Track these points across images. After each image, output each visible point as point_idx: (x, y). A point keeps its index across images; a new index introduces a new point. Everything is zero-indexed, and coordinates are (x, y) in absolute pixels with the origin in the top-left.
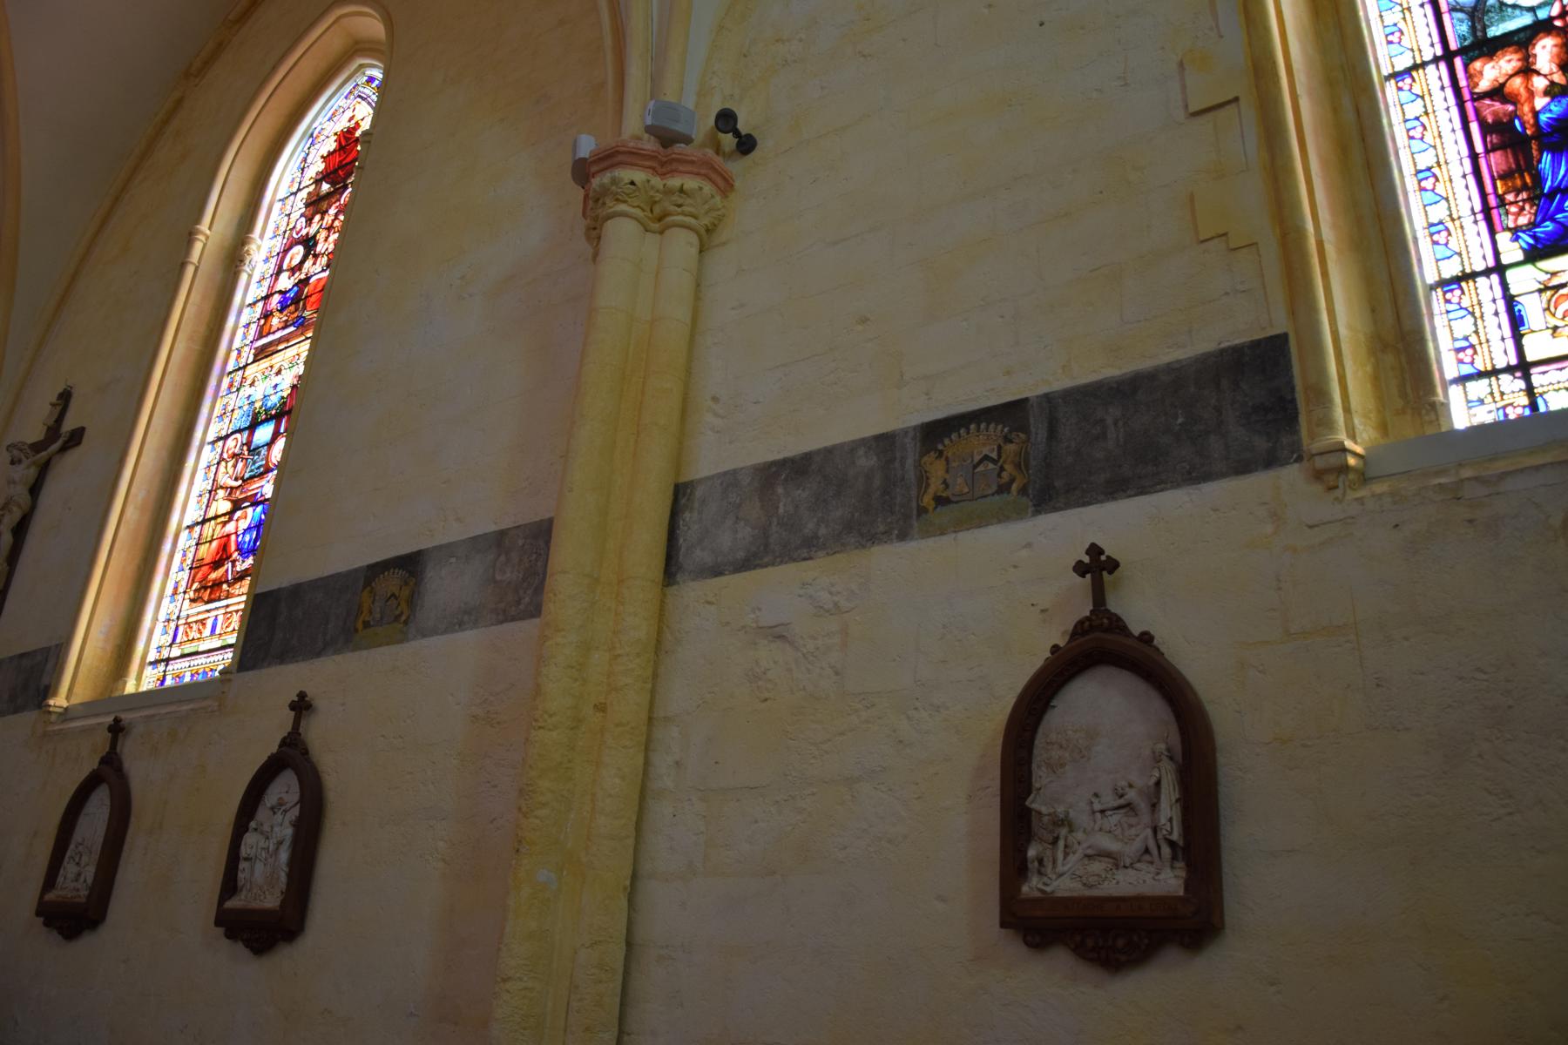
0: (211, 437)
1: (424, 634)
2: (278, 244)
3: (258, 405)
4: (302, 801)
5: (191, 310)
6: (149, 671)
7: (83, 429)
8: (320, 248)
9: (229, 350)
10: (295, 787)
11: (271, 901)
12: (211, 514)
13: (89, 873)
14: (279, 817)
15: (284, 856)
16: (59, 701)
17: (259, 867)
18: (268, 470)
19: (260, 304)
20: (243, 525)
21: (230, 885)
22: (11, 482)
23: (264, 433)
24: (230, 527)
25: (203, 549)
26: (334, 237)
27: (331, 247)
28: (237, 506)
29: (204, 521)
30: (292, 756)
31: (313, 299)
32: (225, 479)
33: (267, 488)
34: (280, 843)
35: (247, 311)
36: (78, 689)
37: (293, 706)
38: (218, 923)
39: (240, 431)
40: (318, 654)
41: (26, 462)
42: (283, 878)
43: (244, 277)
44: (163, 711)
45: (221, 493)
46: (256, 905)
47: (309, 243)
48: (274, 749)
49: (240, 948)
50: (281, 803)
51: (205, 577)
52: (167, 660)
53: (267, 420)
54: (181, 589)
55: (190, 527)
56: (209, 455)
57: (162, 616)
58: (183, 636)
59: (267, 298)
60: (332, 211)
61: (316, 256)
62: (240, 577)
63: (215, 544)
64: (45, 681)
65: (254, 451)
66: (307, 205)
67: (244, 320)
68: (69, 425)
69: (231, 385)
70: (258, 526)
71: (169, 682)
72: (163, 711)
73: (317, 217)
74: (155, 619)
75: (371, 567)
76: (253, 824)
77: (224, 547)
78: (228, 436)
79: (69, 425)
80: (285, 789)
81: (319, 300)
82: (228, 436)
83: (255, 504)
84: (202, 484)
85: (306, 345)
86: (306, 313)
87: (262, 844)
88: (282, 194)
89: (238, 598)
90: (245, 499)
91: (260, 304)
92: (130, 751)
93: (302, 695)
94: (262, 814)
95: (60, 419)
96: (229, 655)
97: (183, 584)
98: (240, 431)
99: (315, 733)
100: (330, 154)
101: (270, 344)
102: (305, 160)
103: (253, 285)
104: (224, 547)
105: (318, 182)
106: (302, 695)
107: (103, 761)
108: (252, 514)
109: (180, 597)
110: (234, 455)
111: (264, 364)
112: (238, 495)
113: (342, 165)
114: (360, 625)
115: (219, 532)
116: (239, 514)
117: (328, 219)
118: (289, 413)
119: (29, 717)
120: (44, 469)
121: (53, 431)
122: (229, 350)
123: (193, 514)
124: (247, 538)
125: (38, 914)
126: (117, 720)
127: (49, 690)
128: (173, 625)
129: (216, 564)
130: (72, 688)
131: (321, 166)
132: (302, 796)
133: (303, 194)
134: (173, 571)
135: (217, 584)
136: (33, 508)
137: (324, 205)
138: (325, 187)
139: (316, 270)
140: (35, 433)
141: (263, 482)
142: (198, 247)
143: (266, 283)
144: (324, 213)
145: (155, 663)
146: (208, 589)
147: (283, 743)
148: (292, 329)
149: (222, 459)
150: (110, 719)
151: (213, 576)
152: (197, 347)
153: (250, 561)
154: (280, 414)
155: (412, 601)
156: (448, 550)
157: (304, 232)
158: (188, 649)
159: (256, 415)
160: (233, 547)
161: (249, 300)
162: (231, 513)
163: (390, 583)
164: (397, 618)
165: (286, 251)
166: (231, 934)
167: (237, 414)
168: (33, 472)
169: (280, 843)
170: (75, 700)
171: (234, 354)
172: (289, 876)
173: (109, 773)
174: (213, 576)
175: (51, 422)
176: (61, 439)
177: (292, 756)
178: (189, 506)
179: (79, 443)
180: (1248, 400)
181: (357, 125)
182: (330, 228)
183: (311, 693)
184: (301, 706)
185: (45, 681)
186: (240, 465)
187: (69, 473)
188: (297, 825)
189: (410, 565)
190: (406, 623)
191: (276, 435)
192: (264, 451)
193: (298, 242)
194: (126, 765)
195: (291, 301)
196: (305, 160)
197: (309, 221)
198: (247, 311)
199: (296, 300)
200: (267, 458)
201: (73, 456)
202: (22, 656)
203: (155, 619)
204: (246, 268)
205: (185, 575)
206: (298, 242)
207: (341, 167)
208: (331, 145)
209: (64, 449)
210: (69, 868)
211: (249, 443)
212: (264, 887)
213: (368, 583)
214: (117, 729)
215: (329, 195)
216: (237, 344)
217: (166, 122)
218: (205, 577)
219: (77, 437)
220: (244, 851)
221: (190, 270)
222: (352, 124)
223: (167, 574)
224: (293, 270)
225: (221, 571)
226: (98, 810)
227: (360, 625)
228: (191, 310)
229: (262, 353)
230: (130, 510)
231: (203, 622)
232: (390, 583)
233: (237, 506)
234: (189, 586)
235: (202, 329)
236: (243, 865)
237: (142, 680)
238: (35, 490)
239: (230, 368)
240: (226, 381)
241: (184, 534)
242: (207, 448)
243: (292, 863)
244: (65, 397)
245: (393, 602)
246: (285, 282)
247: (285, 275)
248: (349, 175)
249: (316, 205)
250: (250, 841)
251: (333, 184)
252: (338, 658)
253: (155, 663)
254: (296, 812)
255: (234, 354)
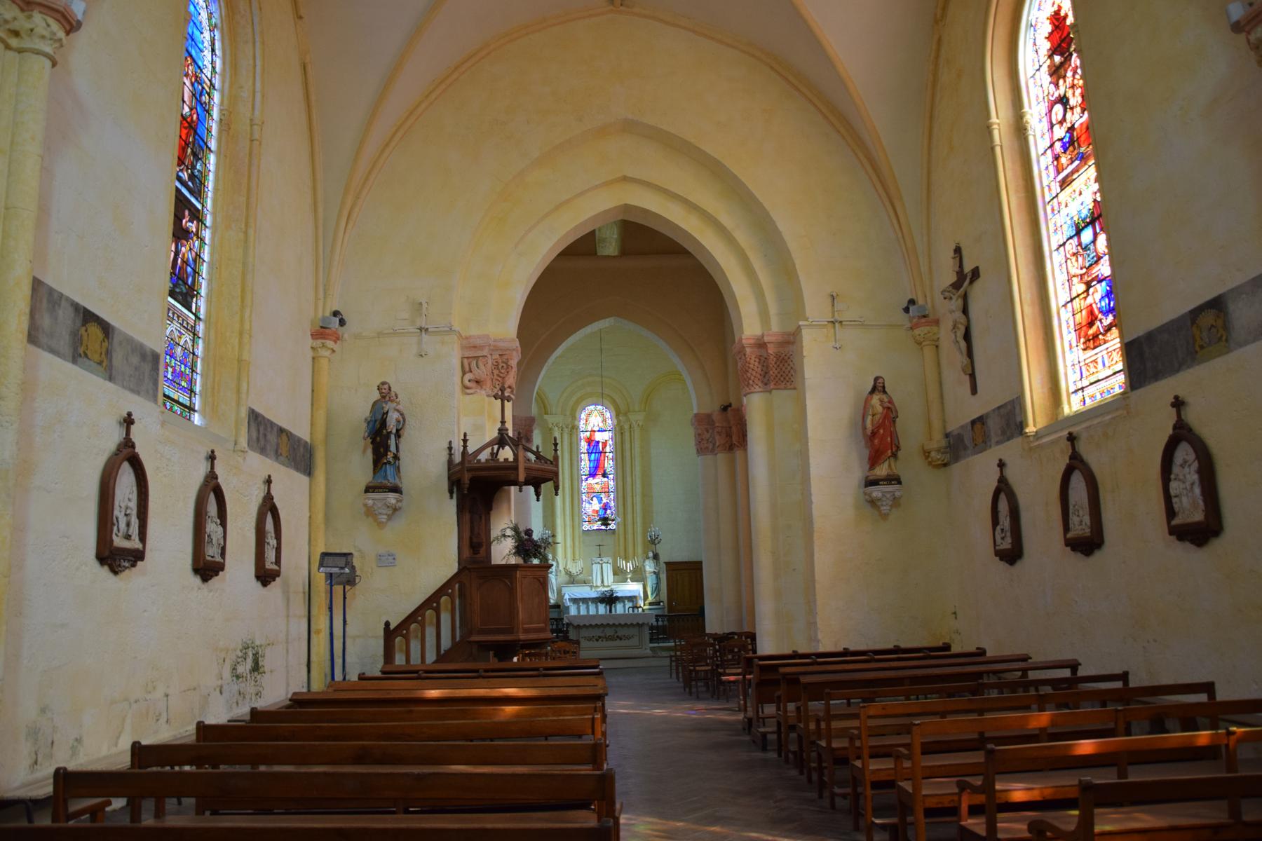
0: (1054, 246)
1: (1241, 346)
2: (1043, 108)
3: (1076, 218)
4: (1197, 457)
5: (1009, 174)
6: (1073, 397)
7: (977, 268)
8: (1072, 102)
9: (1042, 188)
10: (1191, 450)
11: (1198, 516)
12: (1074, 295)
13: (1087, 519)
14: (1187, 469)
15: (1197, 490)
16: (1030, 429)
17: (1185, 500)
18: (1099, 258)
19: (1049, 152)
20: (1098, 296)
21: (1171, 512)
22: (952, 312)
23: (1087, 235)
24: (1090, 300)
25: (1078, 317)
26: (1078, 91)
27: (1080, 100)
28: (1088, 285)
29: (1072, 300)
30: (1182, 433)
31: (1082, 139)
32: (1073, 271)
33: (1104, 269)
34: (1193, 484)
35: (1042, 158)
36: (1038, 419)
37: (1173, 405)
38: (1171, 533)
39: (1071, 238)
40: (1178, 371)
41: (954, 298)
42: (1201, 503)
43: (1031, 139)
44: (1096, 421)
45: (1075, 280)
46: (1190, 520)
47: (1063, 100)
48: (1170, 431)
49: (1188, 545)
50: (1185, 462)
51: (1086, 334)
52: (1082, 389)
53: (1086, 227)
54: (1074, 344)
55: (1065, 306)
56: (1058, 258)
57: (1069, 363)
58: (1090, 375)
59: (1052, 146)
60: (1069, 74)
61: (1072, 108)
62: (1108, 329)
63: (1084, 312)
64: (1018, 419)
65: (1086, 248)
66: (1051, 75)
67: (1043, 167)
68: (968, 268)
69: (1053, 210)
70: (1108, 294)
71: (1088, 402)
72: (1096, 421)
73: (1061, 82)
74: (1065, 366)
75: (1192, 312)
76: (1172, 477)
77: (1091, 312)
78: (1064, 244)
79: (968, 268)
80: (1184, 453)
81: (1088, 138)
82: (1064, 244)
83: (1100, 281)
84: (1061, 277)
85: (1090, 172)
86: (1082, 150)
87: (1182, 486)
88: (1030, 72)
89: (1114, 341)
90: (1093, 280)
91: (1049, 152)
92: (1083, 448)
93: (1176, 398)
94: (1176, 469)
95: (961, 266)
96: (1121, 378)
97: (1074, 344)
98: (1071, 238)
99: (1192, 416)
100: (1051, 34)
101: (1067, 176)
102: (1035, 44)
103: (1040, 138)
104: (1091, 312)
105: (1050, 57)
106: (1176, 398)
107: (1071, 458)
108: (1101, 288)
109: (1075, 349)
110: (1074, 254)
111: (1068, 190)
112: (1086, 278)
113: (1061, 40)
114: (1197, 348)
115: (1084, 304)
116: (1091, 290)
117: (1069, 80)
118: (1100, 216)
119: (1017, 441)
120: (965, 297)
121: (961, 275)
122: (1042, 188)
123: (1063, 297)
124: (1103, 304)
125: (1067, 545)
126: (1070, 434)
127: (1021, 426)
128: (1077, 368)
129: (1091, 324)
130: (1035, 420)
131: (1048, 45)
132: (1196, 452)
133: (1045, 69)
134: (1066, 336)
135: (1095, 337)
136: (968, 321)
137: (1062, 71)
138: (1057, 59)
139: (1078, 118)
140: (953, 278)
141: (1100, 266)
142: (996, 133)
143: (1047, 137)
144: (1064, 77)
145: (1076, 391)
146: (1092, 341)
147: (1175, 427)
148: (1077, 162)
149: (1067, 259)
150: (1065, 433)
151: (1091, 332)
152: (1022, 195)
153: (1110, 318)
154: (1094, 219)
155: (1226, 327)
156: (1237, 291)
157: (1056, 95)
158: (1093, 379)
159: (1077, 225)
160: (1096, 312)
161: (1041, 151)
162: (1087, 291)
163: (1208, 319)
164: (1220, 339)
165: (1050, 111)
166: (1073, 549)
167: (1065, 227)
168: (960, 302)
169: (1193, 484)
170: (1040, 426)
171: (1046, 189)
172: (1205, 501)
173: (1076, 463)
174: (1091, 332)
175: (957, 269)
176: (965, 279)
177: (1182, 433)
178: (1059, 292)
179: (978, 276)
180: (1010, 417)
181: (1060, 8)
182: (1073, 86)
183: (1181, 394)
184: (1178, 404)
185: (1018, 419)
186: (1080, 259)
187: (980, 295)
188: (1199, 472)
189: (1217, 304)
190: (1227, 340)
191: (1095, 235)
192: (1092, 247)
193: (1055, 103)
194: (1085, 457)
195: (1070, 143)
196: (1035, 44)
197: (1057, 85)
198: (1042, 158)
199: (1071, 142)
200: (1096, 251)
201: (978, 284)
202: (999, 408)
203: (1065, 366)
204: (1030, 132)
205: (1073, 336)
206: (1055, 103)
207: (1063, 41)
208: (1049, 28)
209: (971, 282)
210: (1074, 520)
211: (1080, 244)
212: (1191, 509)
213: (1193, 322)
214: (1072, 438)
215: (1062, 64)
216: (1045, 183)
217: (937, 57)
218: (1086, 334)
219: (976, 273)
220: (1173, 492)
221: (998, 150)
222: (1056, 8)
223: (1062, 338)
224: (1061, 123)
225: (1095, 328)
226: (1078, 485)
227: (1197, 348)
228: (1009, 174)
229: (1064, 184)
230: (1026, 309)
231: (1095, 361)
232: (1208, 319)
233: (1088, 285)
234: (1078, 341)
235: (1021, 182)
236: (1174, 500)
237: (1073, 405)
238: (965, 311)
239: (1047, 199)
240: (1049, 208)
241: (1063, 310)
242: (1055, 254)
243: (1203, 493)
244: (958, 250)
245: (1213, 330)
246: (1060, 132)
247: (1056, 128)
248: (1069, 46)
249: (1057, 73)
250: (1174, 487)
251: (1061, 55)
252: (1191, 370)
253: (1076, 391)
254: (1196, 465)
255: (1046, 189)
